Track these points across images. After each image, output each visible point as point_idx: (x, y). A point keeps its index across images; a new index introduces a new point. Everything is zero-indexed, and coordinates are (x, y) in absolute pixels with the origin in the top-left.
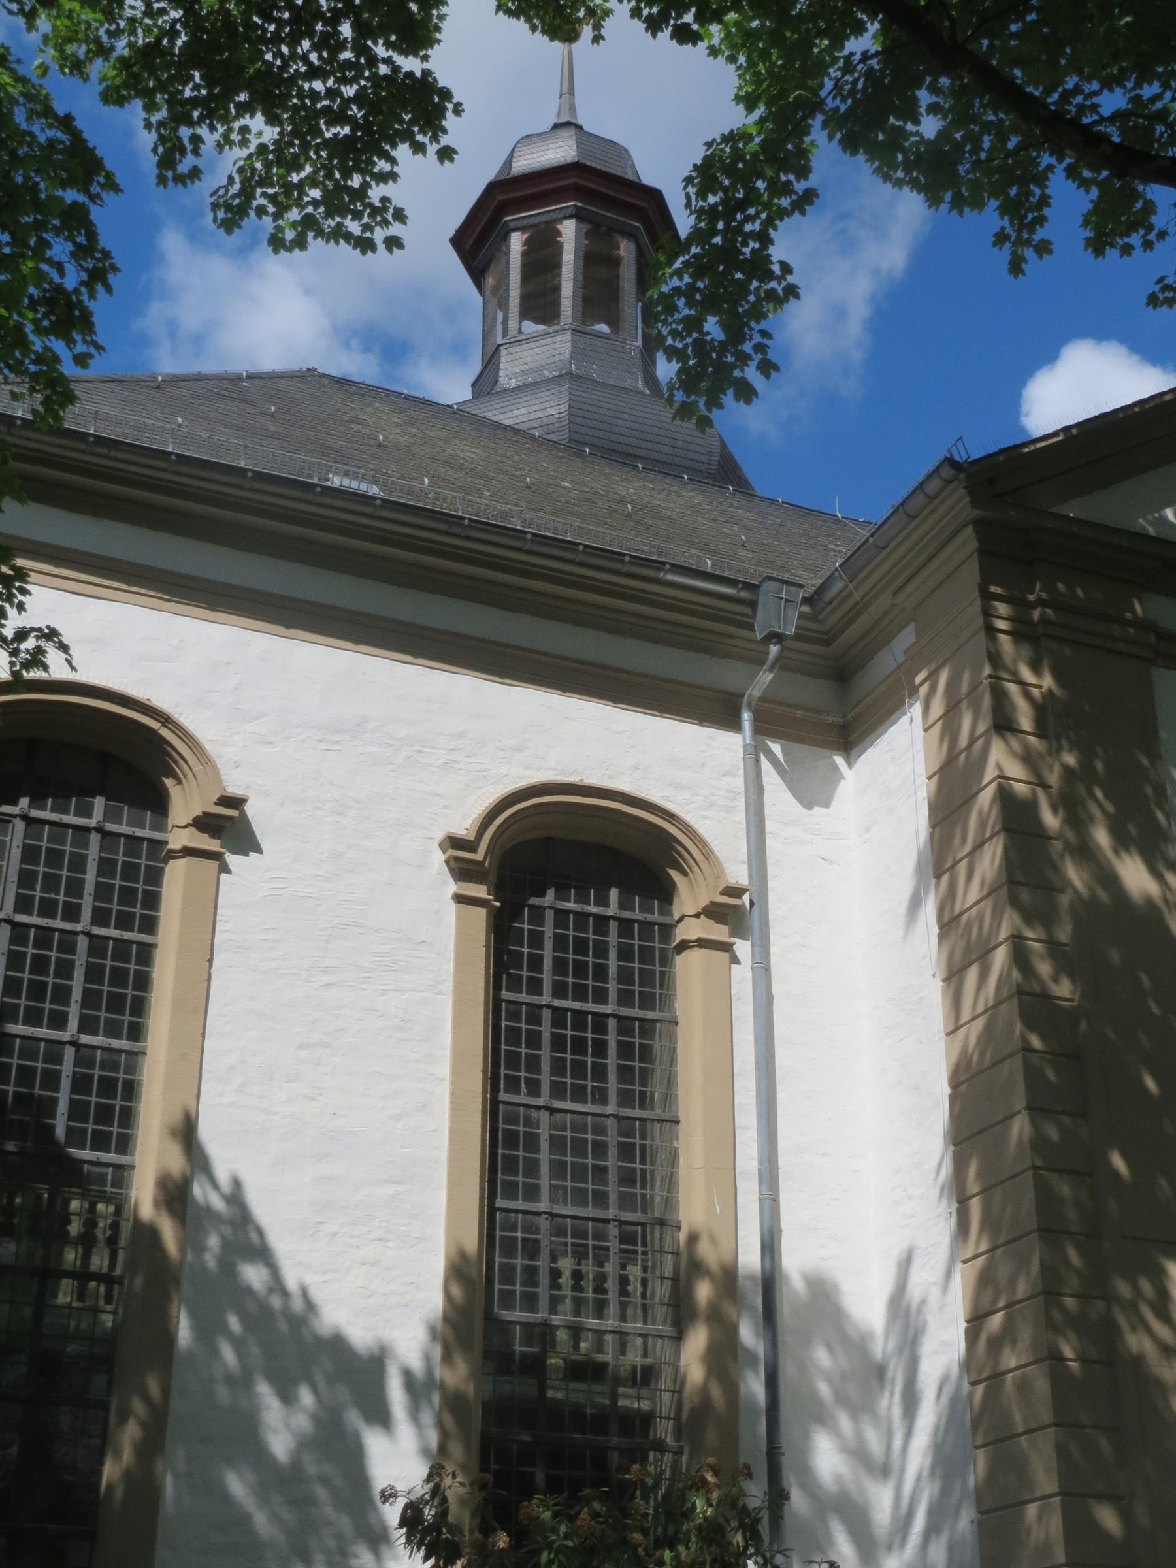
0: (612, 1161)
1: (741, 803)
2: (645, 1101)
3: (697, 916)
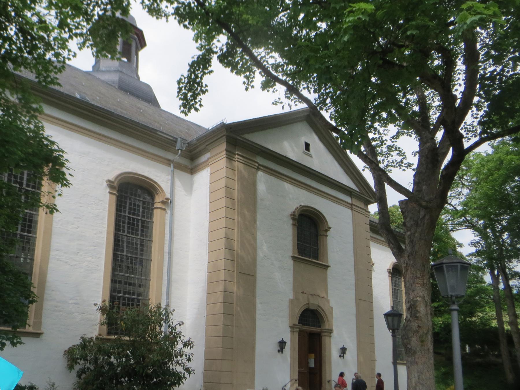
0: (139, 247)
1: (170, 182)
2: (146, 236)
3: (159, 202)
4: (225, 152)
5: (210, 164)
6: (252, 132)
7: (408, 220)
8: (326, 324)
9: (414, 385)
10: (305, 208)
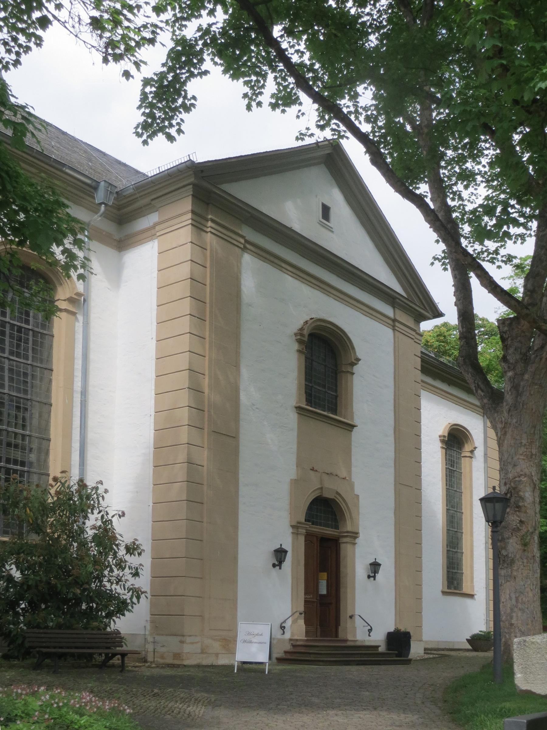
2: (41, 361)
3: (65, 300)
4: (190, 215)
5: (158, 234)
6: (237, 180)
7: (511, 351)
8: (348, 523)
9: (509, 611)
10: (319, 323)
